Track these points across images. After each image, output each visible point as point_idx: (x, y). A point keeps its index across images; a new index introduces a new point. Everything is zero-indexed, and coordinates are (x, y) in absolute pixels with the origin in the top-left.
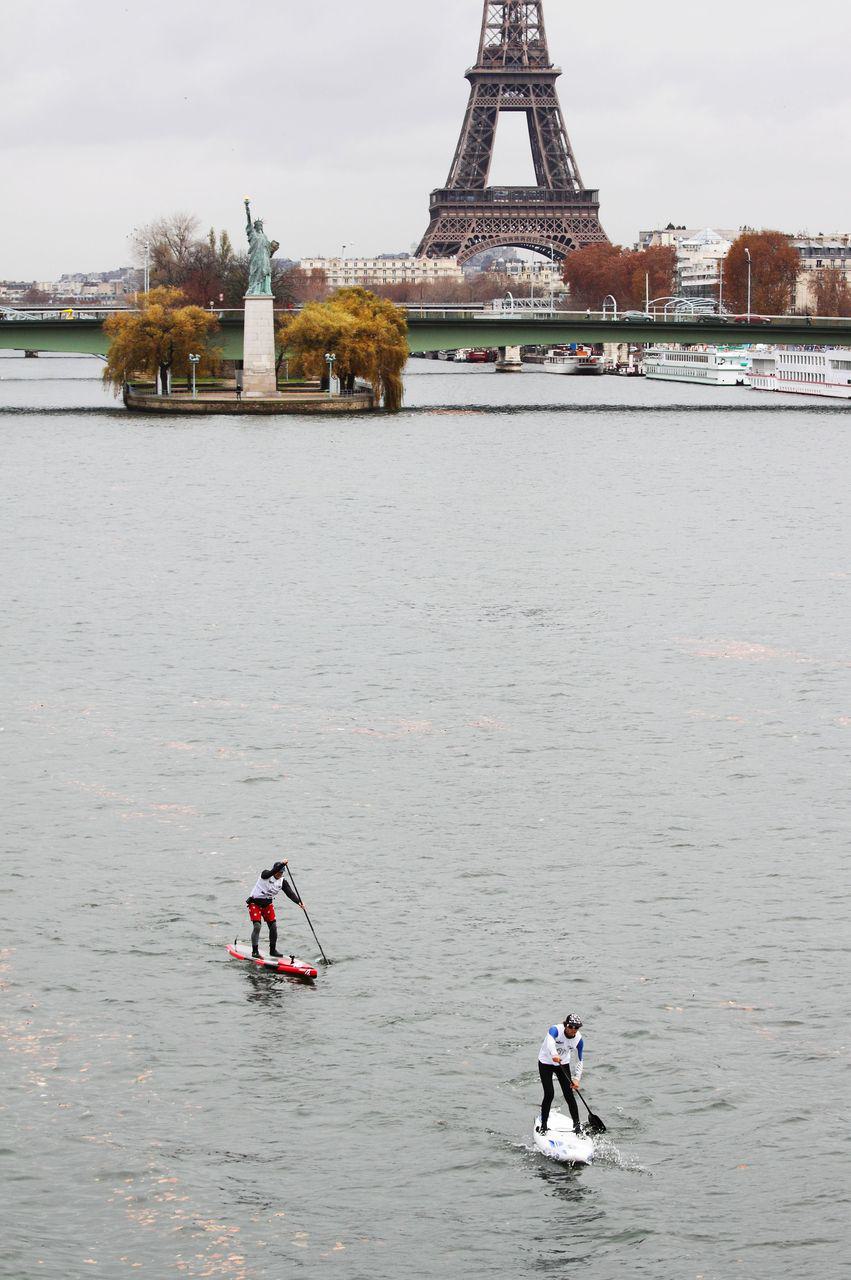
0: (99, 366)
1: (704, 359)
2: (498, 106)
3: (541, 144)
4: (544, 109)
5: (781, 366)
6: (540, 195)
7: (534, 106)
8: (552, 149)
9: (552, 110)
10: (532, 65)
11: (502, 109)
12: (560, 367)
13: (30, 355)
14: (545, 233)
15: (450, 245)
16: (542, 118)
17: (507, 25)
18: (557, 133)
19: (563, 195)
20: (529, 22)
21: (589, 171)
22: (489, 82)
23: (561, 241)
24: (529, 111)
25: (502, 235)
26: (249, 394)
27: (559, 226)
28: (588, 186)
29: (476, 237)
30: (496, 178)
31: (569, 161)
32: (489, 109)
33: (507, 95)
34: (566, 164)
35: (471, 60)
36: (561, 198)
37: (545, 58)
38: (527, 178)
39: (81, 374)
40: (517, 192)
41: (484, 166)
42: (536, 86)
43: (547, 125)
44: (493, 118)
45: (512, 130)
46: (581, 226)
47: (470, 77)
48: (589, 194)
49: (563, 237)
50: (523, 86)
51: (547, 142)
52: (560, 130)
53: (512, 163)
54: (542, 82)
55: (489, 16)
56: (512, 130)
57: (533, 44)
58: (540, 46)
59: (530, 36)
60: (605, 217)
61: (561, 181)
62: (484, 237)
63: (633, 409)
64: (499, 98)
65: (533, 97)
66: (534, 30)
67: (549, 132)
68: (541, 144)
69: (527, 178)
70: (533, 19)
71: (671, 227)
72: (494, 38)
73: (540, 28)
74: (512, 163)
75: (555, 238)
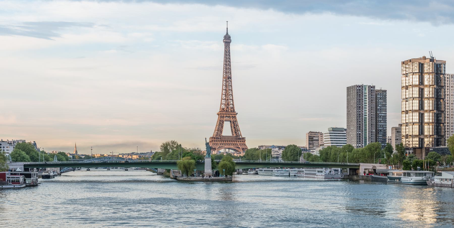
1: (272, 171)
5: (305, 172)
10: (231, 98)
12: (252, 173)
13: (127, 170)
16: (233, 123)
24: (231, 121)
28: (243, 137)
30: (224, 134)
35: (218, 110)
36: (237, 138)
37: (234, 111)
41: (221, 132)
44: (223, 122)
47: (218, 114)
48: (243, 138)
51: (234, 128)
52: (237, 125)
53: (227, 131)
57: (231, 108)
58: (233, 108)
60: (246, 143)
70: (231, 103)
72: (223, 106)
73: (233, 104)
74: (227, 131)
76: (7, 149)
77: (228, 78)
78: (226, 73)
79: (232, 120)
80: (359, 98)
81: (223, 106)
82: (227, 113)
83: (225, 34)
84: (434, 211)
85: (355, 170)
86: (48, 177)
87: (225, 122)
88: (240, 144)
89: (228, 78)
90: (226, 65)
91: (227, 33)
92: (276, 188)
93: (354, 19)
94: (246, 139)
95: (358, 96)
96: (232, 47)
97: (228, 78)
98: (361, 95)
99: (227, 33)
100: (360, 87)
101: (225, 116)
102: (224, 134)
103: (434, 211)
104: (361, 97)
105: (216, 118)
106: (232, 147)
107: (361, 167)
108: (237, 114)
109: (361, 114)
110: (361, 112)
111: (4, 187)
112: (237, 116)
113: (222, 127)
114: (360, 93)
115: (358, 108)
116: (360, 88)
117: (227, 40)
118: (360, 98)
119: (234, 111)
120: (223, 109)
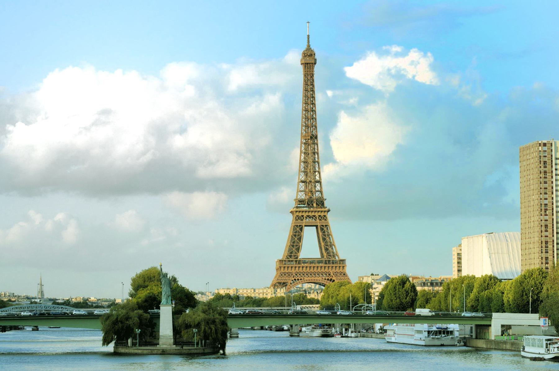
0: (100, 336)
2: (304, 225)
3: (324, 251)
4: (323, 226)
6: (320, 262)
7: (319, 225)
8: (326, 242)
9: (326, 226)
10: (317, 178)
11: (305, 226)
14: (324, 278)
15: (284, 283)
16: (322, 229)
17: (307, 190)
18: (331, 246)
19: (331, 262)
20: (317, 189)
21: (342, 250)
22: (300, 214)
23: (330, 281)
24: (317, 226)
25: (306, 278)
26: (162, 346)
27: (329, 275)
28: (341, 258)
29: (295, 280)
30: (302, 255)
31: (316, 156)
32: (300, 226)
33: (307, 220)
34: (332, 249)
36: (330, 259)
38: (316, 255)
39: (93, 340)
40: (312, 261)
41: (298, 249)
42: (320, 216)
43: (324, 232)
44: (301, 229)
45: (310, 236)
46: (338, 274)
47: (291, 212)
48: (343, 261)
49: (331, 279)
50: (314, 216)
53: (310, 248)
54: (322, 214)
55: (300, 187)
56: (310, 236)
59: (317, 195)
61: (330, 256)
62: (298, 280)
63: (321, 351)
64: (304, 221)
65: (318, 220)
66: (319, 193)
67: (325, 235)
68: (324, 251)
69: (316, 255)
71: (372, 275)
72: (302, 196)
73: (321, 192)
74: (310, 248)
75: (328, 280)
76: (545, 190)
77: (311, 138)
78: (307, 126)
79: (318, 223)
80: (543, 169)
83: (305, 47)
84: (348, 298)
85: (482, 330)
88: (336, 274)
90: (306, 110)
91: (309, 46)
94: (347, 263)
95: (542, 165)
98: (549, 162)
99: (309, 46)
100: (545, 145)
101: (305, 215)
102: (302, 255)
103: (348, 298)
104: (549, 167)
105: (288, 221)
106: (319, 279)
107: (493, 323)
108: (329, 211)
109: (550, 205)
110: (550, 199)
112: (329, 216)
113: (300, 239)
114: (546, 159)
115: (543, 191)
116: (545, 148)
117: (309, 62)
118: (546, 169)
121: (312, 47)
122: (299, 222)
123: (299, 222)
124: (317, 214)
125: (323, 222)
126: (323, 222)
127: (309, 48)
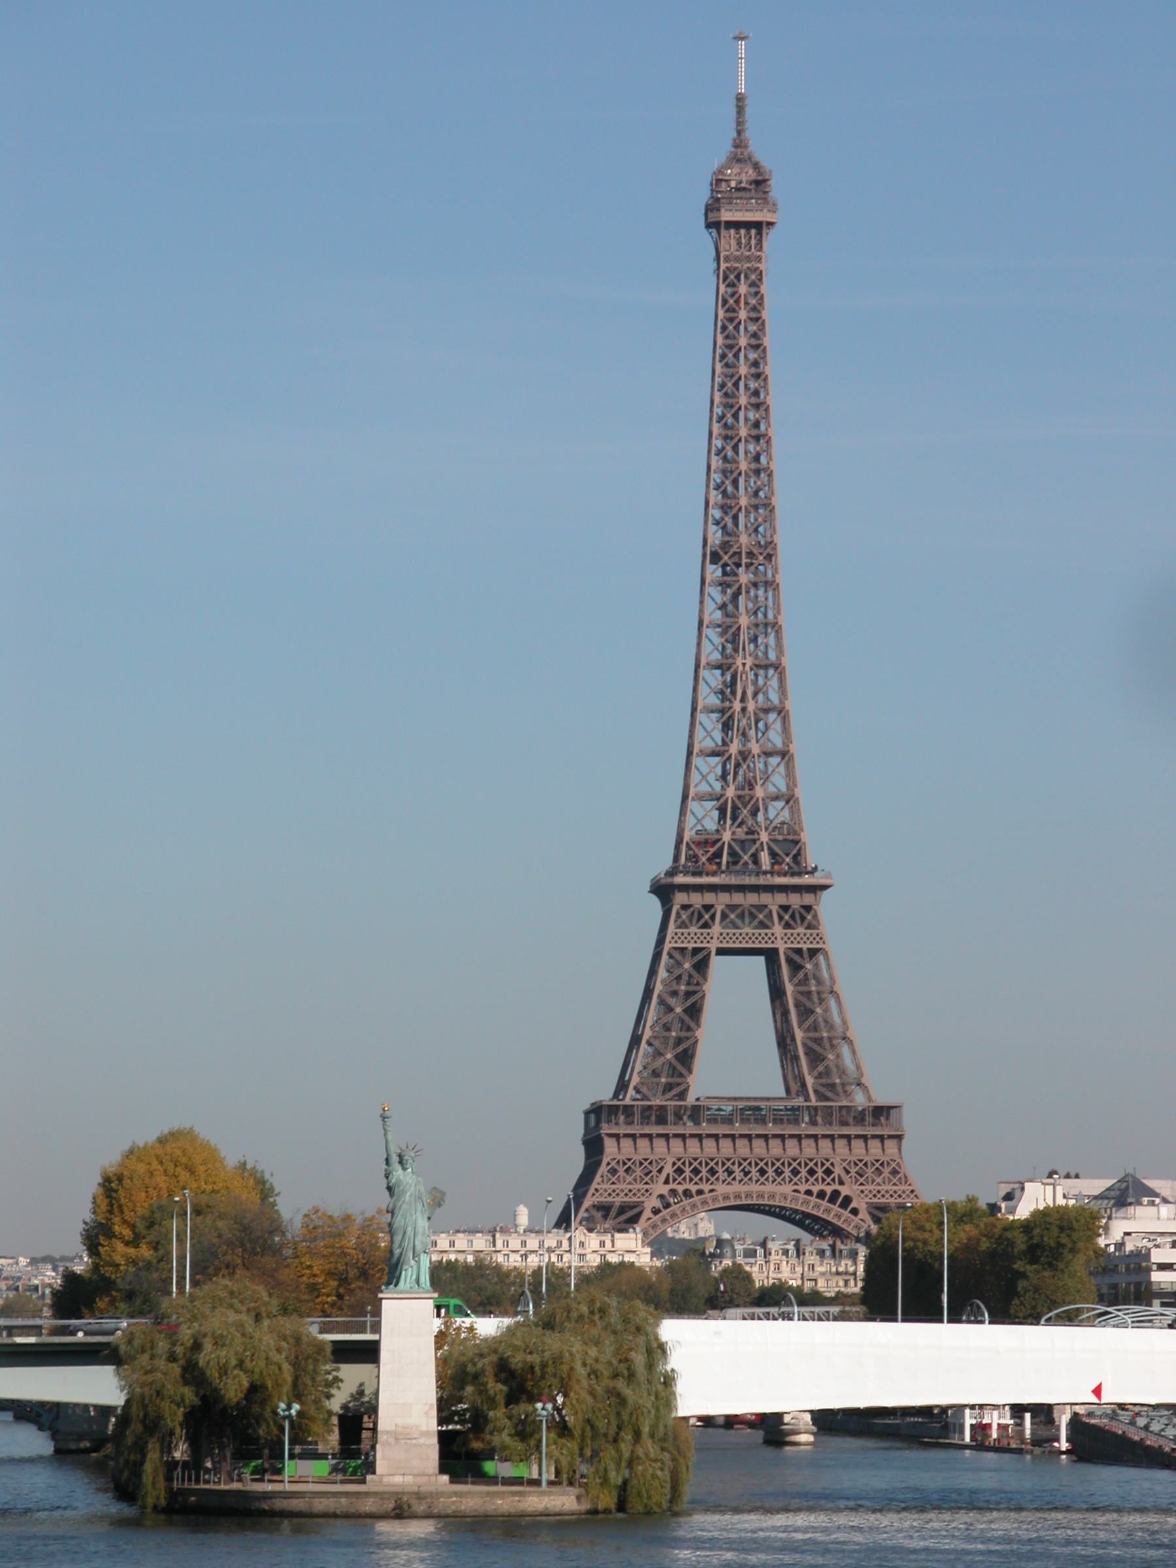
16: (795, 967)
22: (696, 900)
24: (771, 955)
30: (707, 1081)
36: (820, 1091)
40: (753, 1112)
44: (702, 966)
45: (737, 994)
48: (881, 1112)
53: (738, 1051)
54: (795, 900)
56: (737, 994)
72: (705, 817)
73: (790, 799)
74: (738, 1051)
79: (780, 938)
81: (705, 817)
82: (739, 880)
86: (486, 1545)
87: (716, 961)
89: (739, 558)
91: (739, 143)
92: (876, 1445)
93: (913, 1404)
96: (749, 112)
97: (739, 558)
99: (739, 143)
101: (721, 901)
106: (782, 1192)
111: (941, 1441)
112: (826, 906)
113: (694, 1011)
117: (738, 211)
119: (798, 866)
120: (706, 841)
121: (757, 148)
122: (692, 936)
123: (692, 936)
124: (773, 902)
125: (801, 938)
126: (801, 938)
127: (740, 154)
